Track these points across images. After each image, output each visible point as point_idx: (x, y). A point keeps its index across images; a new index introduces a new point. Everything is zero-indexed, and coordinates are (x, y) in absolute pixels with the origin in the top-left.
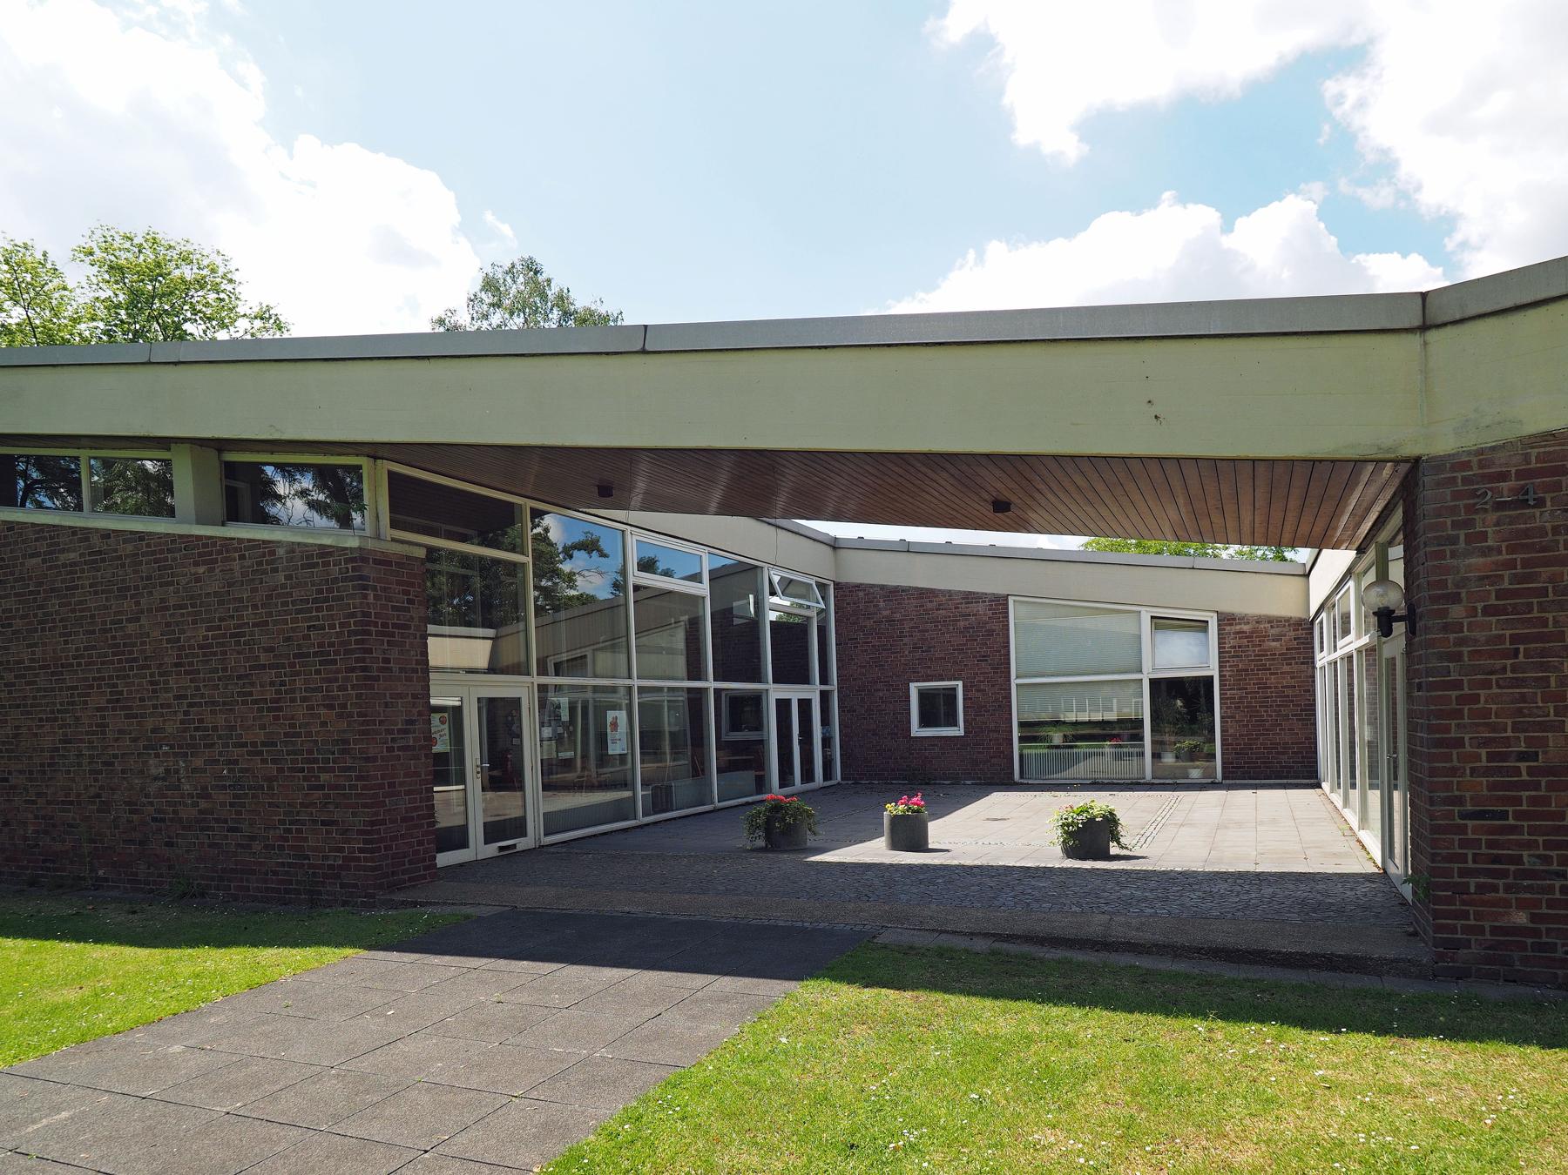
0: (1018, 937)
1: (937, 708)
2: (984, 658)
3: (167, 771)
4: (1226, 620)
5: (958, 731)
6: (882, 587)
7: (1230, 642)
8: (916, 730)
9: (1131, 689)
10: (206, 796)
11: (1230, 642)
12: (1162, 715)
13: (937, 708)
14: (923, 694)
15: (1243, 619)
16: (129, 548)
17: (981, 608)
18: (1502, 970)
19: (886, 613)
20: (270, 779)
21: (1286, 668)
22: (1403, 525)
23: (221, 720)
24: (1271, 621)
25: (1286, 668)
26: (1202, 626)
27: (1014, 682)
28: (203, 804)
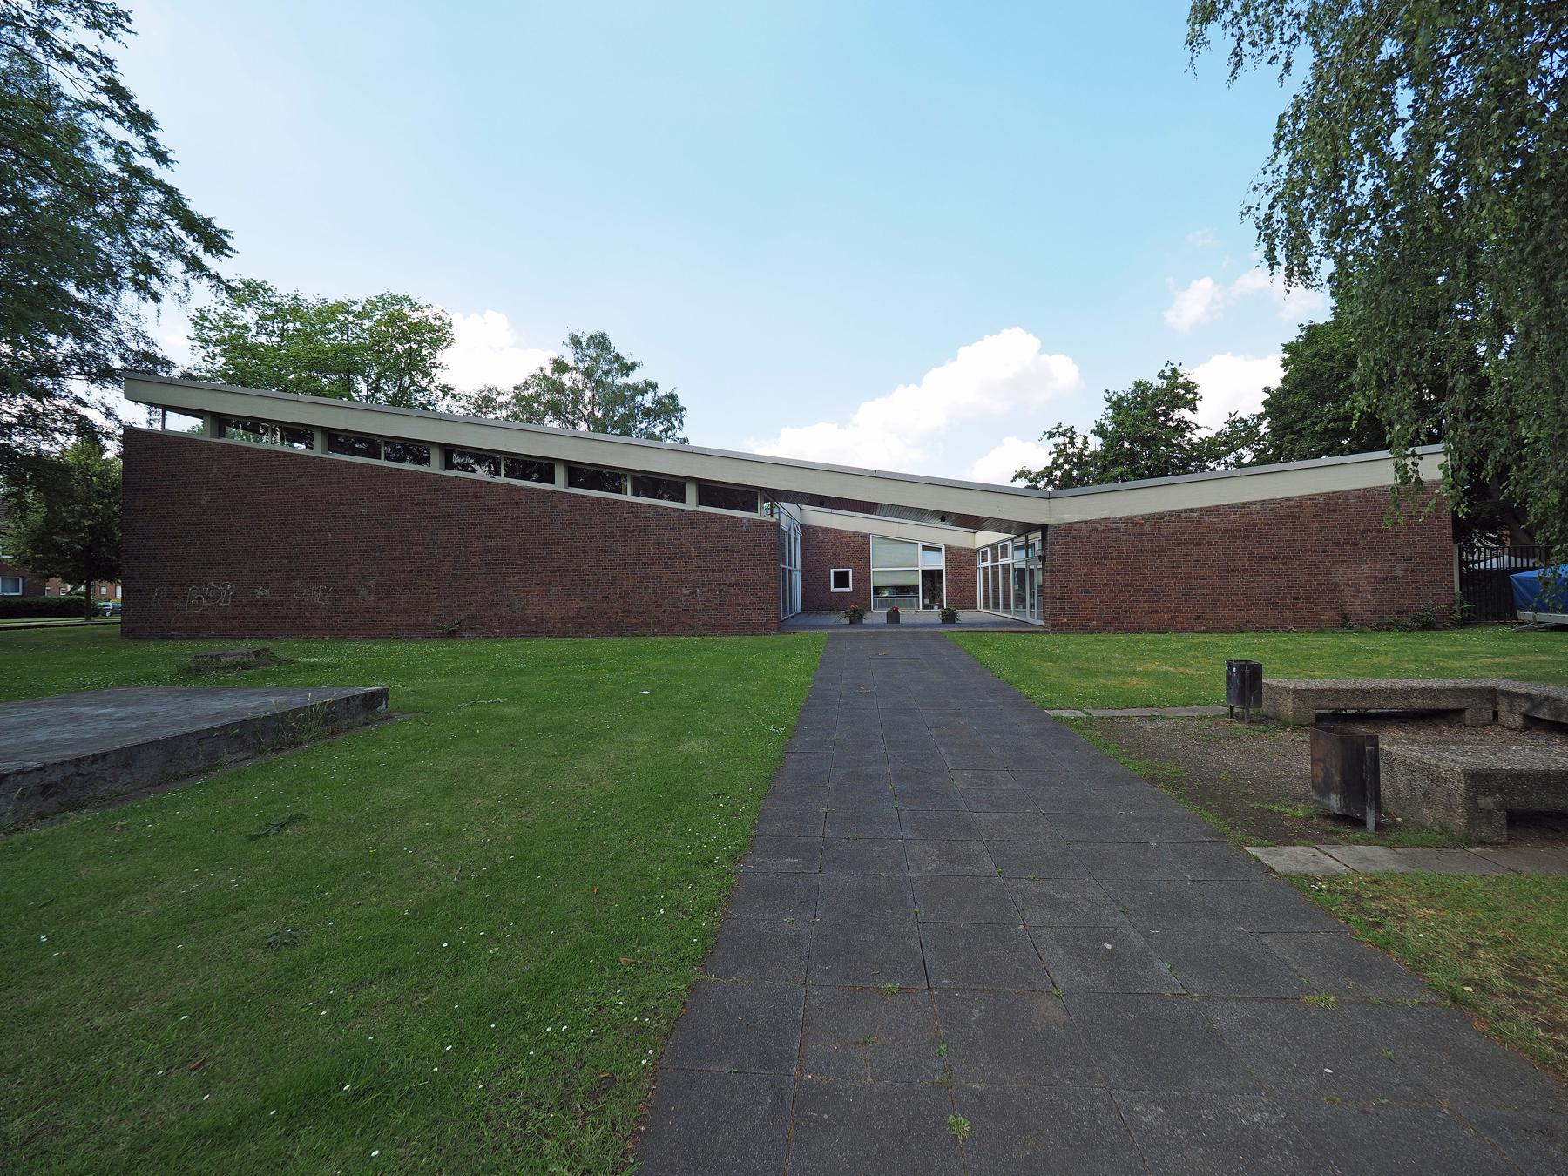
0: (928, 625)
1: (841, 580)
2: (861, 560)
3: (691, 593)
4: (948, 548)
5: (849, 590)
6: (820, 527)
7: (949, 557)
8: (833, 590)
9: (916, 573)
10: (708, 600)
11: (949, 557)
12: (509, 641)
13: (841, 580)
14: (835, 573)
15: (953, 548)
16: (677, 514)
17: (860, 538)
18: (1028, 616)
19: (822, 539)
20: (737, 595)
21: (968, 567)
22: (139, 112)
23: (716, 575)
24: (963, 549)
25: (968, 567)
26: (939, 550)
27: (872, 570)
28: (707, 604)
